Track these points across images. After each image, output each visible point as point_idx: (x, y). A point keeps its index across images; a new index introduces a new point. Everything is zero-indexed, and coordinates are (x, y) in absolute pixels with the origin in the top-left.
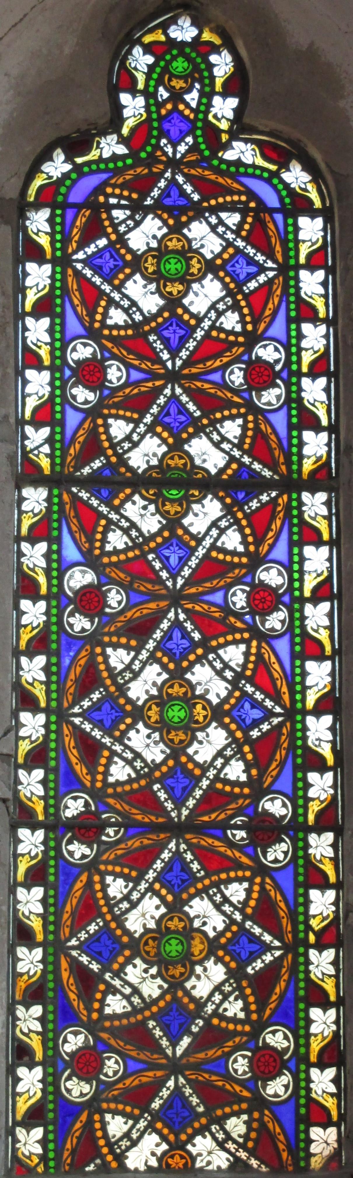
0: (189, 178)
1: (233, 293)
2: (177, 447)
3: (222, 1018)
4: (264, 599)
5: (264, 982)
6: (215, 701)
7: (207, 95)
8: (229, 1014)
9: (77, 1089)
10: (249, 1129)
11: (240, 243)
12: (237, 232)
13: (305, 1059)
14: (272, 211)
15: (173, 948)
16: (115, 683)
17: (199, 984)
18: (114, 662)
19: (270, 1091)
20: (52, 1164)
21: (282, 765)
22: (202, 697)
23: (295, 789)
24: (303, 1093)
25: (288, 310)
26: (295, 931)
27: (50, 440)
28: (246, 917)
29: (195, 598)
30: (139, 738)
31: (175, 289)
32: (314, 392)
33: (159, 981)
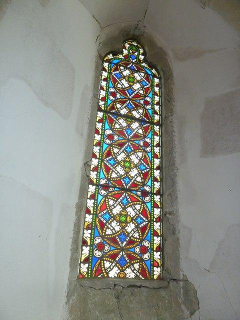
0: (135, 66)
1: (142, 87)
2: (130, 112)
3: (134, 237)
4: (146, 145)
5: (143, 229)
6: (136, 163)
7: (139, 54)
8: (135, 237)
9: (98, 254)
10: (140, 267)
11: (144, 79)
12: (144, 77)
13: (153, 249)
14: (150, 75)
15: (123, 219)
16: (114, 155)
17: (128, 228)
18: (115, 151)
19: (144, 257)
20: (90, 274)
21: (149, 179)
22: (133, 162)
23: (151, 185)
24: (152, 258)
25: (151, 231)
26: (151, 218)
27: (104, 104)
28: (140, 213)
29: (133, 141)
30: (119, 169)
31: (131, 84)
32: (157, 108)
33: (119, 227)
